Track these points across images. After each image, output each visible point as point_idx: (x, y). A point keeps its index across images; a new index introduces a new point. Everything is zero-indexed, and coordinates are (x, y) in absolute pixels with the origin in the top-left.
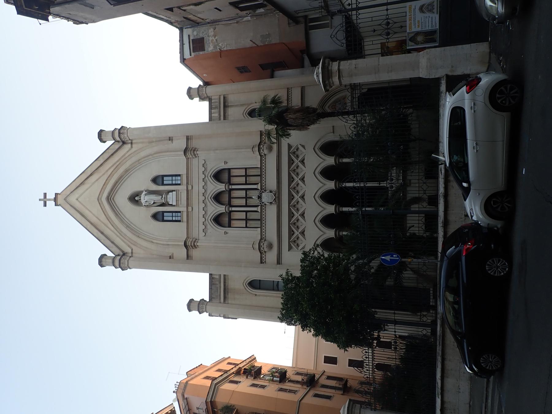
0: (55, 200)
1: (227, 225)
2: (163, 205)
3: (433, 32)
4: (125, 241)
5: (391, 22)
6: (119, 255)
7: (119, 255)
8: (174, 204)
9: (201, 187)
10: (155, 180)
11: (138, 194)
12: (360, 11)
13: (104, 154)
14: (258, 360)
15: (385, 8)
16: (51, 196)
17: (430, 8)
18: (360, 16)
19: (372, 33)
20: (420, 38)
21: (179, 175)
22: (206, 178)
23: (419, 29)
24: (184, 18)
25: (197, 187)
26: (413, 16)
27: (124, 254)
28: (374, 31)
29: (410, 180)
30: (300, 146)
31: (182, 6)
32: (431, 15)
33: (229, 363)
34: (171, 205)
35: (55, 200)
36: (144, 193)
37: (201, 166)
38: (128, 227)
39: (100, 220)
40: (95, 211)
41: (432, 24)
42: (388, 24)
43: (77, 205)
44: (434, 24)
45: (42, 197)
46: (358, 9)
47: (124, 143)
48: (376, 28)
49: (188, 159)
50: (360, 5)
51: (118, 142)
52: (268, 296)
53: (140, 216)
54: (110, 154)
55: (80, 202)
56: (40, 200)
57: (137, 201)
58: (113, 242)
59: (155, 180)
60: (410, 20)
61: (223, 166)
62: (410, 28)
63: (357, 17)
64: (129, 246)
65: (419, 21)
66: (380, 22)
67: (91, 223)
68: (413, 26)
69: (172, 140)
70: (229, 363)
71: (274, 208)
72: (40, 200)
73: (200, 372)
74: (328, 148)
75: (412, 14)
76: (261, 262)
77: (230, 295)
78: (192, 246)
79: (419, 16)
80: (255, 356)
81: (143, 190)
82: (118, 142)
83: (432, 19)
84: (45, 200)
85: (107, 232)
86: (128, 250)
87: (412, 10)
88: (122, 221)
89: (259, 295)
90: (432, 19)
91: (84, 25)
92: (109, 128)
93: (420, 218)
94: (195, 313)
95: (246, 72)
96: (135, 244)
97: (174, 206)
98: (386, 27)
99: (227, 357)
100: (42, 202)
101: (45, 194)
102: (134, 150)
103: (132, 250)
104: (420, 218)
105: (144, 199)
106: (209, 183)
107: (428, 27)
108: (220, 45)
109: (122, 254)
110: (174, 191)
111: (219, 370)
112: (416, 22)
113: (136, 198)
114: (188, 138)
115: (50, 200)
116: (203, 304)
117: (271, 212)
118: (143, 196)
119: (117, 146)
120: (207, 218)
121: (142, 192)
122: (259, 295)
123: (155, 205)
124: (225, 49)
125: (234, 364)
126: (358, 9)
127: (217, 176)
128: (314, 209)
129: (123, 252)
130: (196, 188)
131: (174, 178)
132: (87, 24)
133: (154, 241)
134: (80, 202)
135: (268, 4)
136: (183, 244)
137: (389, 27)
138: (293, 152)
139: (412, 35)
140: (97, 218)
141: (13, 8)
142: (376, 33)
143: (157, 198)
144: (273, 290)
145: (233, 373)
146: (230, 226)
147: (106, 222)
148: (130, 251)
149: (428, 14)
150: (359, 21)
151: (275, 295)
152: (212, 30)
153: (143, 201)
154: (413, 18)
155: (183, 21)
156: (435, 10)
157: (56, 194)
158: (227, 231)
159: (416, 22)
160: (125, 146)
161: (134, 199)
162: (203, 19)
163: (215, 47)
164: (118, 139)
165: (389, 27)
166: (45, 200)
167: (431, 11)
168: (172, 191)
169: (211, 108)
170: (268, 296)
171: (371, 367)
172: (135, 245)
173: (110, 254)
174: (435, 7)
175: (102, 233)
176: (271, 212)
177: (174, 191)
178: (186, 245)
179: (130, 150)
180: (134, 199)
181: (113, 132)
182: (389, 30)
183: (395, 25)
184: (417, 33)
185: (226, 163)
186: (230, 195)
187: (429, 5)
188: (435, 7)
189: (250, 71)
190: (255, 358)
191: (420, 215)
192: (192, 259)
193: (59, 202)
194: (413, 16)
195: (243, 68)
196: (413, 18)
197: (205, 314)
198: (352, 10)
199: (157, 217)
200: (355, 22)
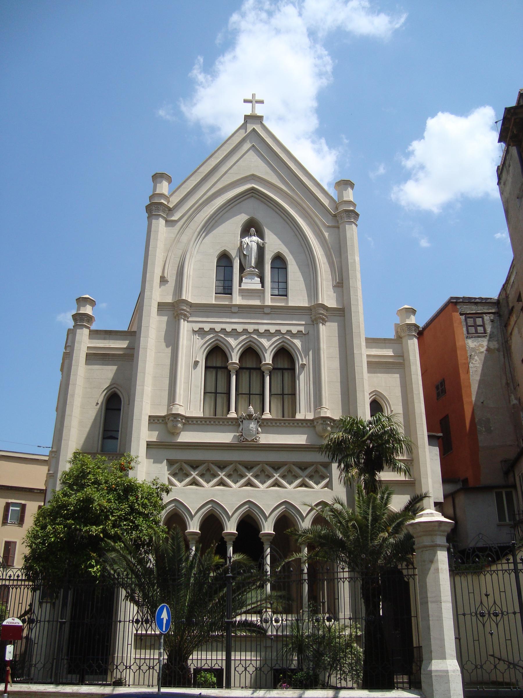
1: (209, 364)
2: (242, 269)
5: (499, 618)
8: (244, 286)
11: (260, 234)
12: (513, 575)
16: (259, 110)
18: (506, 574)
19: (484, 592)
24: (513, 307)
28: (487, 595)
42: (496, 615)
45: (257, 98)
46: (516, 571)
48: (491, 598)
51: (337, 208)
63: (506, 570)
66: (498, 602)
81: (266, 240)
82: (337, 208)
91: (496, 181)
93: (219, 662)
95: (438, 395)
97: (240, 286)
98: (492, 612)
100: (250, 98)
104: (219, 662)
105: (253, 241)
108: (476, 358)
109: (171, 206)
110: (263, 286)
118: (255, 238)
123: (242, 257)
124: (471, 365)
126: (516, 571)
128: (232, 497)
132: (498, 184)
135: (252, 696)
137: (492, 615)
141: (513, 103)
142: (484, 598)
144: (105, 430)
146: (207, 368)
147: (219, 186)
148: (175, 218)
150: (500, 573)
152: (497, 346)
153: (246, 240)
155: (508, 306)
162: (511, 334)
163: (473, 350)
164: (341, 209)
165: (492, 615)
168: (262, 282)
171: (15, 583)
177: (263, 286)
179: (324, 224)
182: (487, 615)
183: (494, 625)
189: (437, 399)
191: (224, 662)
195: (444, 391)
198: (515, 563)
199: (224, 260)
200: (494, 568)
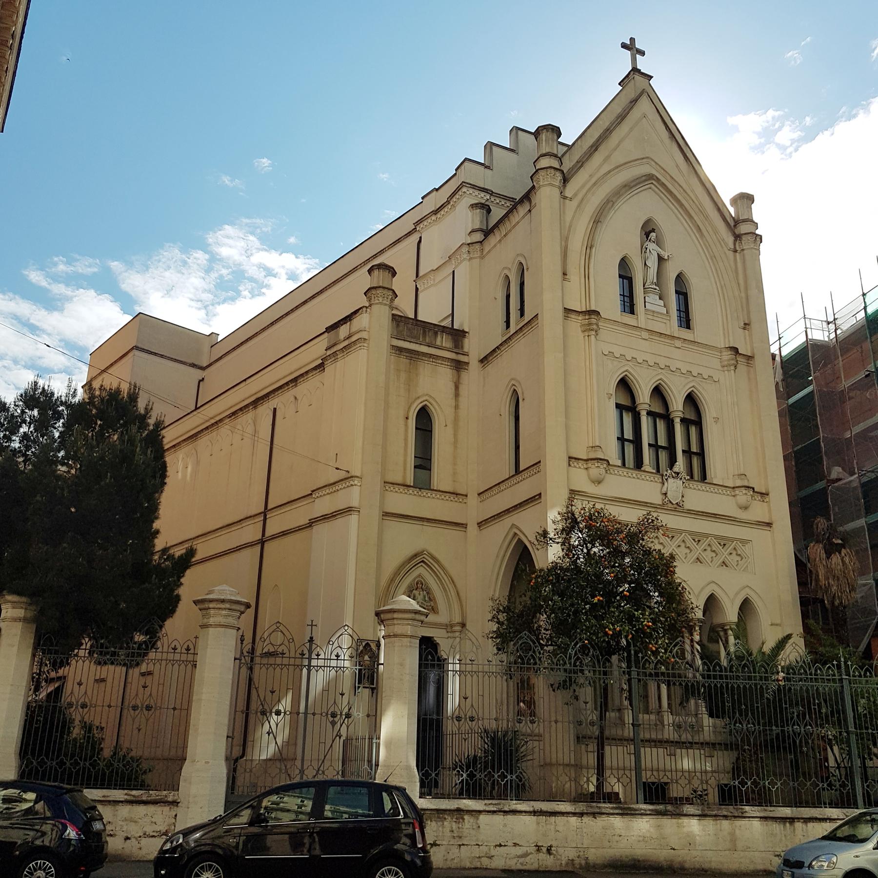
4: (584, 191)
9: (679, 365)
15: (310, 717)
22: (692, 378)
27: (565, 180)
28: (272, 692)
49: (720, 350)
50: (313, 671)
63: (651, 675)
69: (744, 329)
77: (404, 360)
78: (590, 324)
85: (598, 158)
89: (406, 425)
92: (758, 212)
114: (749, 358)
122: (406, 425)
130: (677, 354)
136: (593, 308)
160: (732, 239)
172: (579, 206)
185: (717, 420)
186: (660, 416)
192: (566, 317)
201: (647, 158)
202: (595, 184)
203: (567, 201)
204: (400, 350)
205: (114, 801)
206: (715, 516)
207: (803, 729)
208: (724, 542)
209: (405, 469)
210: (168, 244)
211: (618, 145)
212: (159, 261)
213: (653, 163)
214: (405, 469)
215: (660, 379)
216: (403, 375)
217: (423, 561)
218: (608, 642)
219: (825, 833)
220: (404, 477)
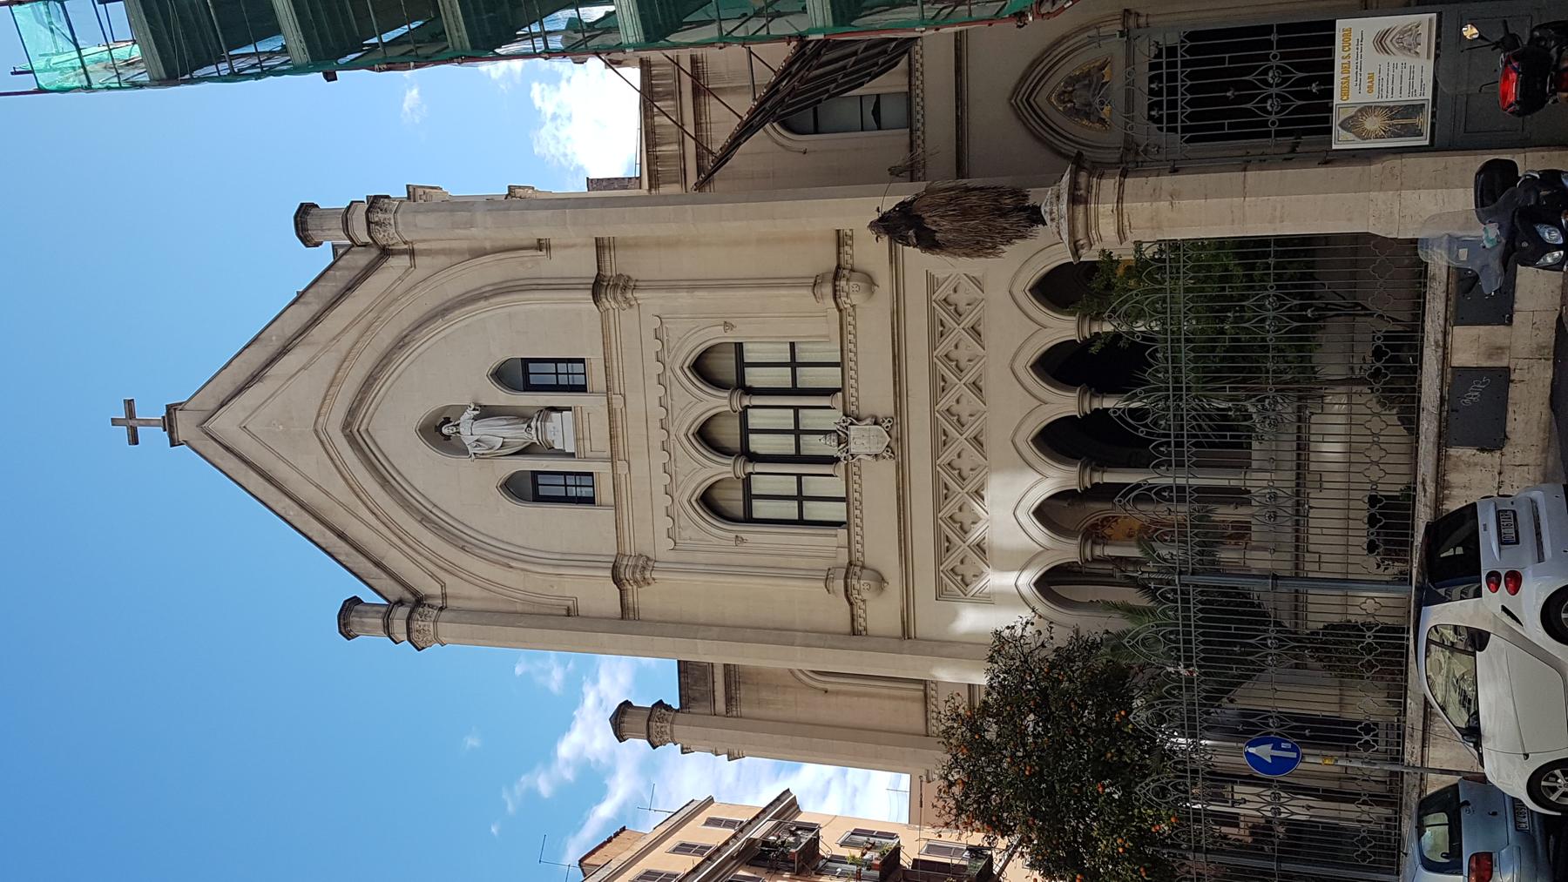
0: (169, 423)
3: (1414, 109)
4: (419, 559)
6: (401, 602)
7: (401, 602)
10: (501, 375)
13: (320, 283)
14: (804, 808)
17: (1408, 40)
20: (1373, 123)
21: (582, 361)
22: (669, 373)
23: (1372, 98)
25: (642, 401)
26: (1353, 60)
27: (419, 601)
29: (1320, 473)
30: (965, 282)
31: (702, 150)
32: (1410, 60)
33: (712, 822)
34: (562, 454)
35: (169, 423)
36: (470, 413)
37: (649, 335)
38: (424, 520)
39: (327, 493)
40: (311, 469)
41: (1411, 85)
43: (245, 445)
44: (1417, 86)
47: (386, 252)
49: (604, 315)
52: (865, 695)
53: (467, 488)
54: (341, 285)
55: (253, 436)
56: (114, 422)
57: (448, 438)
58: (378, 564)
59: (501, 375)
60: (1346, 69)
61: (716, 335)
62: (1345, 92)
64: (433, 576)
65: (1371, 76)
67: (302, 505)
68: (1353, 89)
69: (548, 248)
70: (712, 822)
71: (888, 467)
72: (114, 422)
73: (627, 855)
74: (1055, 290)
75: (1353, 52)
76: (854, 632)
77: (743, 693)
79: (1373, 60)
80: (794, 792)
83: (1412, 72)
84: (131, 423)
85: (356, 530)
86: (429, 587)
87: (1353, 42)
88: (406, 505)
89: (837, 693)
90: (1412, 72)
92: (332, 199)
94: (638, 745)
96: (453, 570)
99: (701, 798)
101: (129, 404)
102: (418, 274)
103: (443, 586)
105: (469, 430)
106: (676, 389)
107: (1400, 96)
110: (569, 409)
111: (684, 848)
112: (1365, 77)
113: (445, 430)
115: (148, 423)
116: (661, 719)
117: (877, 482)
119: (361, 259)
120: (676, 495)
121: (464, 408)
122: (837, 693)
125: (729, 824)
127: (702, 368)
129: (415, 593)
130: (635, 401)
131: (562, 367)
133: (513, 564)
134: (253, 436)
136: (608, 573)
138: (946, 310)
139: (1352, 112)
140: (318, 486)
143: (517, 434)
145: (731, 858)
149: (1399, 58)
151: (885, 691)
153: (468, 439)
154: (1353, 66)
156: (1422, 49)
157: (169, 407)
158: (744, 536)
159: (1365, 77)
160: (393, 261)
161: (438, 431)
164: (363, 237)
166: (131, 423)
167: (1409, 49)
169: (649, 96)
170: (865, 695)
173: (368, 596)
174: (1424, 39)
175: (341, 536)
176: (877, 482)
177: (569, 409)
178: (617, 580)
180: (438, 431)
181: (346, 215)
184: (1366, 110)
187: (1403, 32)
188: (1424, 39)
190: (794, 802)
193: (181, 434)
194: (1353, 60)
196: (1353, 66)
197: (672, 750)
201: (316, 431)
202: (384, 483)
203: (448, 591)
204: (729, 700)
205: (1425, 718)
206: (896, 358)
207: (1274, 90)
208: (938, 332)
209: (903, 698)
210: (536, 150)
211: (318, 486)
212: (565, 155)
213: (321, 419)
214: (903, 698)
215: (689, 502)
216: (764, 694)
217: (1048, 98)
218: (1100, 795)
219: (1392, 417)
220: (913, 700)
